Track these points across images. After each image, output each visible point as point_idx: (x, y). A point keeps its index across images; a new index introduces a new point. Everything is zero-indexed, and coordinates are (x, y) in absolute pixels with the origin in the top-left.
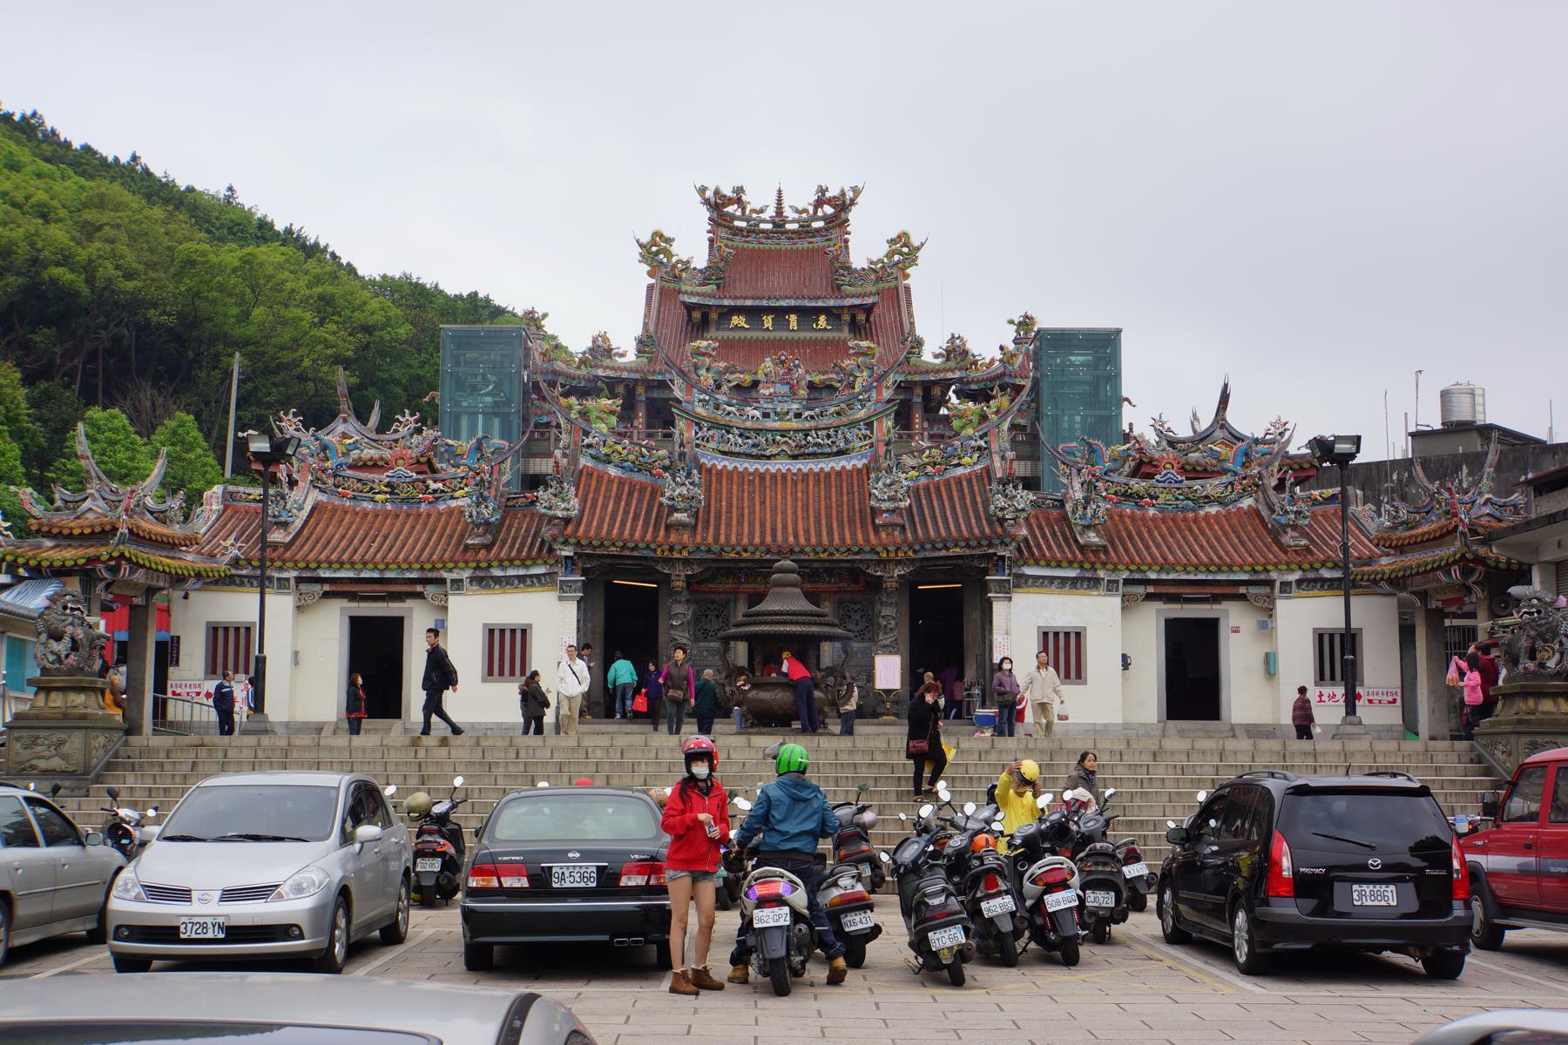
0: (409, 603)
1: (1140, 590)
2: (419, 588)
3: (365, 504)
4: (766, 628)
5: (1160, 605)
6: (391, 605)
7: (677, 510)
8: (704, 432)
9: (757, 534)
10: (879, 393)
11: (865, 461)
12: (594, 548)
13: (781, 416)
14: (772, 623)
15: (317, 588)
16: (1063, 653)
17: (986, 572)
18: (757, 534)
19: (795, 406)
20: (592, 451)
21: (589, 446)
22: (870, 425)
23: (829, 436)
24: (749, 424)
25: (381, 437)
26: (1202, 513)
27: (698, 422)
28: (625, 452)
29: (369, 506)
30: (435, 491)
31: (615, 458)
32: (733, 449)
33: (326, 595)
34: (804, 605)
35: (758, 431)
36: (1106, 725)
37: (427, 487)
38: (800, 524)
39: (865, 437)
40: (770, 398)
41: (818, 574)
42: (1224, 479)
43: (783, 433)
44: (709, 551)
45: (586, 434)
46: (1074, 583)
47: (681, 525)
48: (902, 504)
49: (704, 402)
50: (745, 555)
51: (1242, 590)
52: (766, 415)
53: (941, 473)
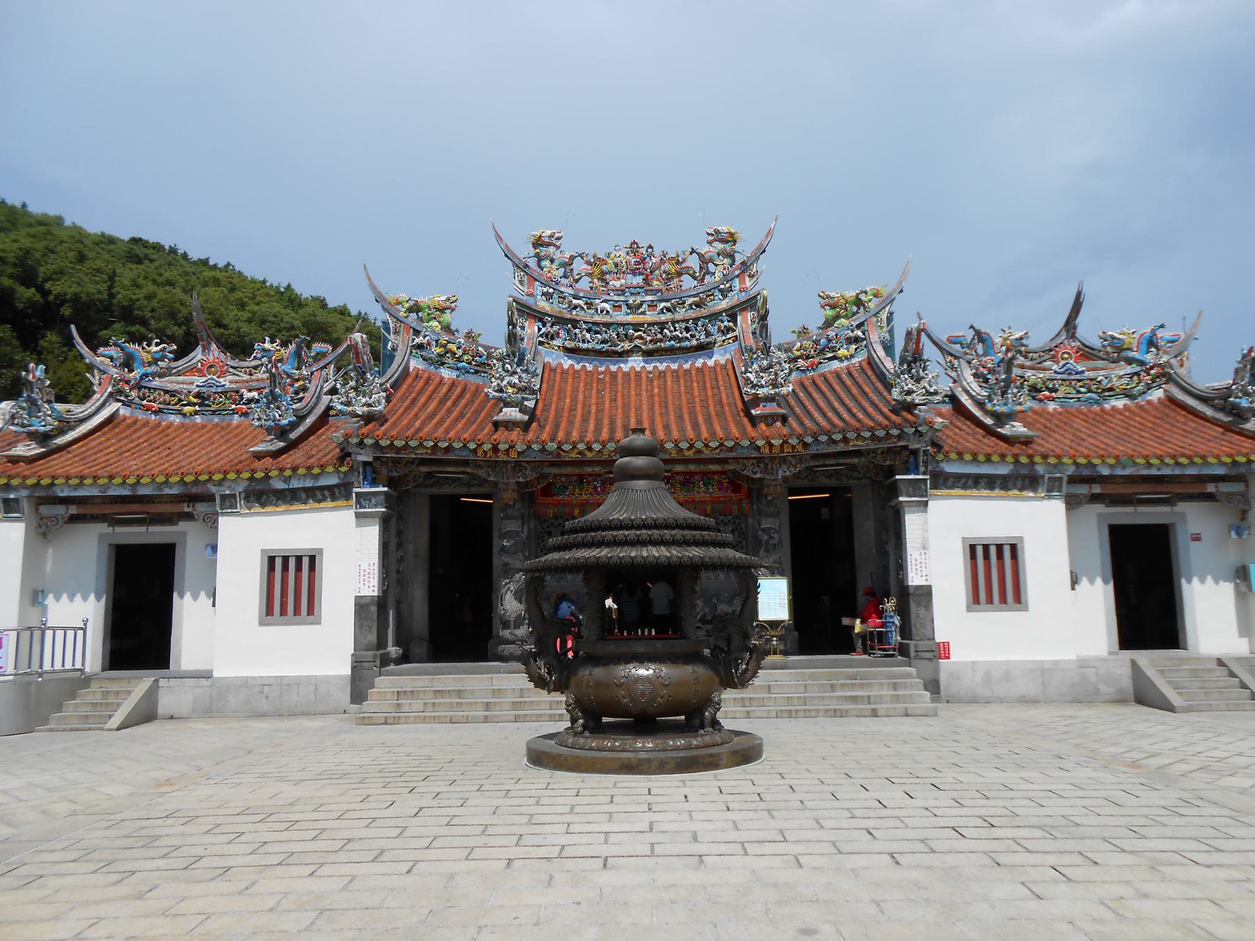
0: (183, 526)
1: (1083, 490)
3: (172, 417)
4: (604, 552)
5: (1100, 508)
6: (152, 529)
7: (507, 405)
9: (605, 430)
11: (728, 356)
14: (615, 543)
15: (60, 510)
16: (996, 573)
17: (891, 472)
18: (605, 430)
19: (649, 298)
21: (420, 347)
22: (733, 318)
24: (597, 318)
26: (1107, 406)
27: (539, 316)
28: (460, 352)
29: (177, 419)
30: (250, 401)
33: (74, 519)
35: (608, 325)
36: (1056, 663)
37: (241, 396)
38: (658, 419)
39: (728, 330)
40: (621, 291)
41: (680, 471)
43: (637, 327)
44: (543, 450)
45: (417, 333)
47: (509, 425)
48: (784, 390)
49: (548, 296)
50: (589, 455)
51: (1211, 488)
52: (617, 307)
53: (813, 367)
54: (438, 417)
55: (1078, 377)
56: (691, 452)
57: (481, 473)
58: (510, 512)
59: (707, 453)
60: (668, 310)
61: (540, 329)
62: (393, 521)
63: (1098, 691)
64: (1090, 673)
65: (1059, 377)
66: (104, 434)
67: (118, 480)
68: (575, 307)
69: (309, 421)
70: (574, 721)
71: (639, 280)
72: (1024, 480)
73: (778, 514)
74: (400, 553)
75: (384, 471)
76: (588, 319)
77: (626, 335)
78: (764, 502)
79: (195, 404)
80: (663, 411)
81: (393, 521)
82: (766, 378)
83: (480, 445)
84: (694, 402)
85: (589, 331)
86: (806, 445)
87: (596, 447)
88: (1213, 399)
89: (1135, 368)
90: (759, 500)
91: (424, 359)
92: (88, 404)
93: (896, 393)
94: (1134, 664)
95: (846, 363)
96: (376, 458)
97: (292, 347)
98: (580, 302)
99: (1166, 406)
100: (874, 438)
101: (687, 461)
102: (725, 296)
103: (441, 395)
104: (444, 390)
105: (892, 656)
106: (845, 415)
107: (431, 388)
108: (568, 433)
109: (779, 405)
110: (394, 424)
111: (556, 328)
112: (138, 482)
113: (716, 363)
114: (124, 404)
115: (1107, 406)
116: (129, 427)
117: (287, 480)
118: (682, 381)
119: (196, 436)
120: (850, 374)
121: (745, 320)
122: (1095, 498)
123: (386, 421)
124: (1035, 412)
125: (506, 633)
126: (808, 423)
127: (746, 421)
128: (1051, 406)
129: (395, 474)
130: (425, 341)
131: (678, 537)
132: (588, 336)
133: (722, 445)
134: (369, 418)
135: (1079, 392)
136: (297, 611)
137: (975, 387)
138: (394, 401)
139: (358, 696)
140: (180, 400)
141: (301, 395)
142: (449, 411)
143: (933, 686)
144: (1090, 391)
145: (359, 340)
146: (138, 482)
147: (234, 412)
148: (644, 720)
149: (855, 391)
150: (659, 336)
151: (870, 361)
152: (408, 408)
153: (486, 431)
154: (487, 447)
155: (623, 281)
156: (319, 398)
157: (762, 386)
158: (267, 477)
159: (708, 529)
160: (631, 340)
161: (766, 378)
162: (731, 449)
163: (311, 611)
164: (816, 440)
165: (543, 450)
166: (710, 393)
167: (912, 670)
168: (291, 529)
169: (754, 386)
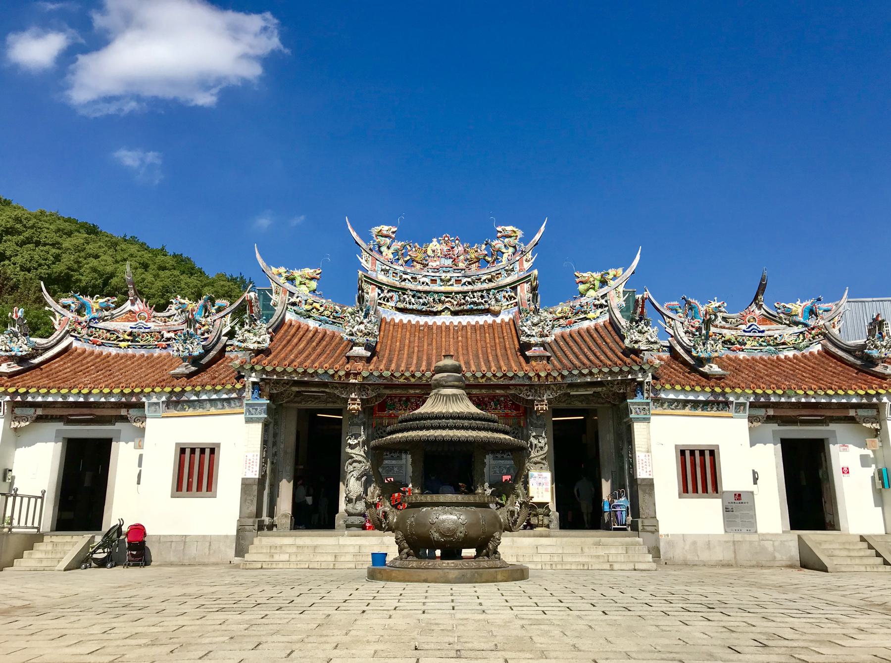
0: (119, 426)
1: (761, 412)
2: (123, 412)
4: (400, 435)
5: (774, 427)
8: (385, 294)
10: (521, 264)
12: (278, 374)
13: (445, 282)
15: (30, 411)
17: (624, 397)
20: (295, 308)
21: (294, 304)
22: (514, 289)
23: (482, 297)
24: (420, 288)
25: (159, 314)
27: (380, 286)
28: (322, 309)
30: (168, 339)
31: (314, 314)
32: (408, 306)
33: (40, 419)
34: (471, 408)
40: (436, 270)
41: (481, 392)
42: (796, 329)
43: (447, 294)
44: (381, 376)
46: (705, 405)
48: (548, 339)
49: (386, 272)
50: (413, 380)
51: (852, 413)
52: (434, 281)
54: (307, 352)
55: (760, 334)
56: (484, 380)
58: (356, 420)
59: (495, 381)
60: (469, 283)
61: (379, 295)
62: (271, 426)
63: (774, 559)
64: (768, 545)
65: (747, 334)
66: (62, 359)
67: (75, 391)
68: (405, 280)
69: (213, 353)
71: (449, 262)
72: (718, 404)
73: (545, 425)
74: (275, 450)
75: (267, 390)
77: (439, 300)
78: (534, 416)
79: (128, 340)
80: (465, 352)
81: (271, 426)
83: (336, 372)
84: (486, 347)
85: (413, 296)
86: (563, 377)
87: (418, 374)
88: (855, 351)
89: (801, 328)
90: (531, 416)
91: (296, 313)
92: (51, 338)
93: (627, 341)
94: (799, 537)
97: (201, 302)
98: (409, 277)
99: (823, 356)
100: (611, 373)
102: (509, 275)
103: (308, 338)
104: (310, 335)
105: (625, 529)
106: (592, 357)
107: (301, 333)
108: (398, 366)
109: (545, 349)
110: (275, 356)
111: (390, 294)
112: (90, 392)
113: (502, 320)
115: (782, 356)
116: (80, 355)
117: (197, 394)
118: (478, 332)
119: (129, 362)
120: (596, 329)
121: (522, 290)
122: (769, 419)
123: (270, 353)
124: (730, 359)
126: (565, 361)
127: (522, 359)
129: (275, 392)
130: (298, 300)
131: (474, 425)
132: (413, 300)
134: (258, 352)
135: (761, 345)
136: (199, 489)
137: (686, 339)
138: (275, 340)
139: (240, 551)
140: (118, 337)
141: (206, 335)
142: (314, 349)
143: (655, 552)
144: (770, 345)
145: (253, 297)
146: (90, 392)
147: (156, 347)
149: (599, 341)
150: (463, 301)
151: (612, 323)
152: (285, 346)
153: (341, 362)
154: (342, 373)
155: (438, 263)
156: (219, 338)
157: (533, 336)
158: (183, 391)
159: (494, 421)
160: (443, 302)
161: (537, 330)
162: (511, 378)
163: (209, 488)
164: (570, 373)
165: (381, 376)
166: (497, 341)
167: (640, 540)
168: (196, 429)
169: (528, 336)
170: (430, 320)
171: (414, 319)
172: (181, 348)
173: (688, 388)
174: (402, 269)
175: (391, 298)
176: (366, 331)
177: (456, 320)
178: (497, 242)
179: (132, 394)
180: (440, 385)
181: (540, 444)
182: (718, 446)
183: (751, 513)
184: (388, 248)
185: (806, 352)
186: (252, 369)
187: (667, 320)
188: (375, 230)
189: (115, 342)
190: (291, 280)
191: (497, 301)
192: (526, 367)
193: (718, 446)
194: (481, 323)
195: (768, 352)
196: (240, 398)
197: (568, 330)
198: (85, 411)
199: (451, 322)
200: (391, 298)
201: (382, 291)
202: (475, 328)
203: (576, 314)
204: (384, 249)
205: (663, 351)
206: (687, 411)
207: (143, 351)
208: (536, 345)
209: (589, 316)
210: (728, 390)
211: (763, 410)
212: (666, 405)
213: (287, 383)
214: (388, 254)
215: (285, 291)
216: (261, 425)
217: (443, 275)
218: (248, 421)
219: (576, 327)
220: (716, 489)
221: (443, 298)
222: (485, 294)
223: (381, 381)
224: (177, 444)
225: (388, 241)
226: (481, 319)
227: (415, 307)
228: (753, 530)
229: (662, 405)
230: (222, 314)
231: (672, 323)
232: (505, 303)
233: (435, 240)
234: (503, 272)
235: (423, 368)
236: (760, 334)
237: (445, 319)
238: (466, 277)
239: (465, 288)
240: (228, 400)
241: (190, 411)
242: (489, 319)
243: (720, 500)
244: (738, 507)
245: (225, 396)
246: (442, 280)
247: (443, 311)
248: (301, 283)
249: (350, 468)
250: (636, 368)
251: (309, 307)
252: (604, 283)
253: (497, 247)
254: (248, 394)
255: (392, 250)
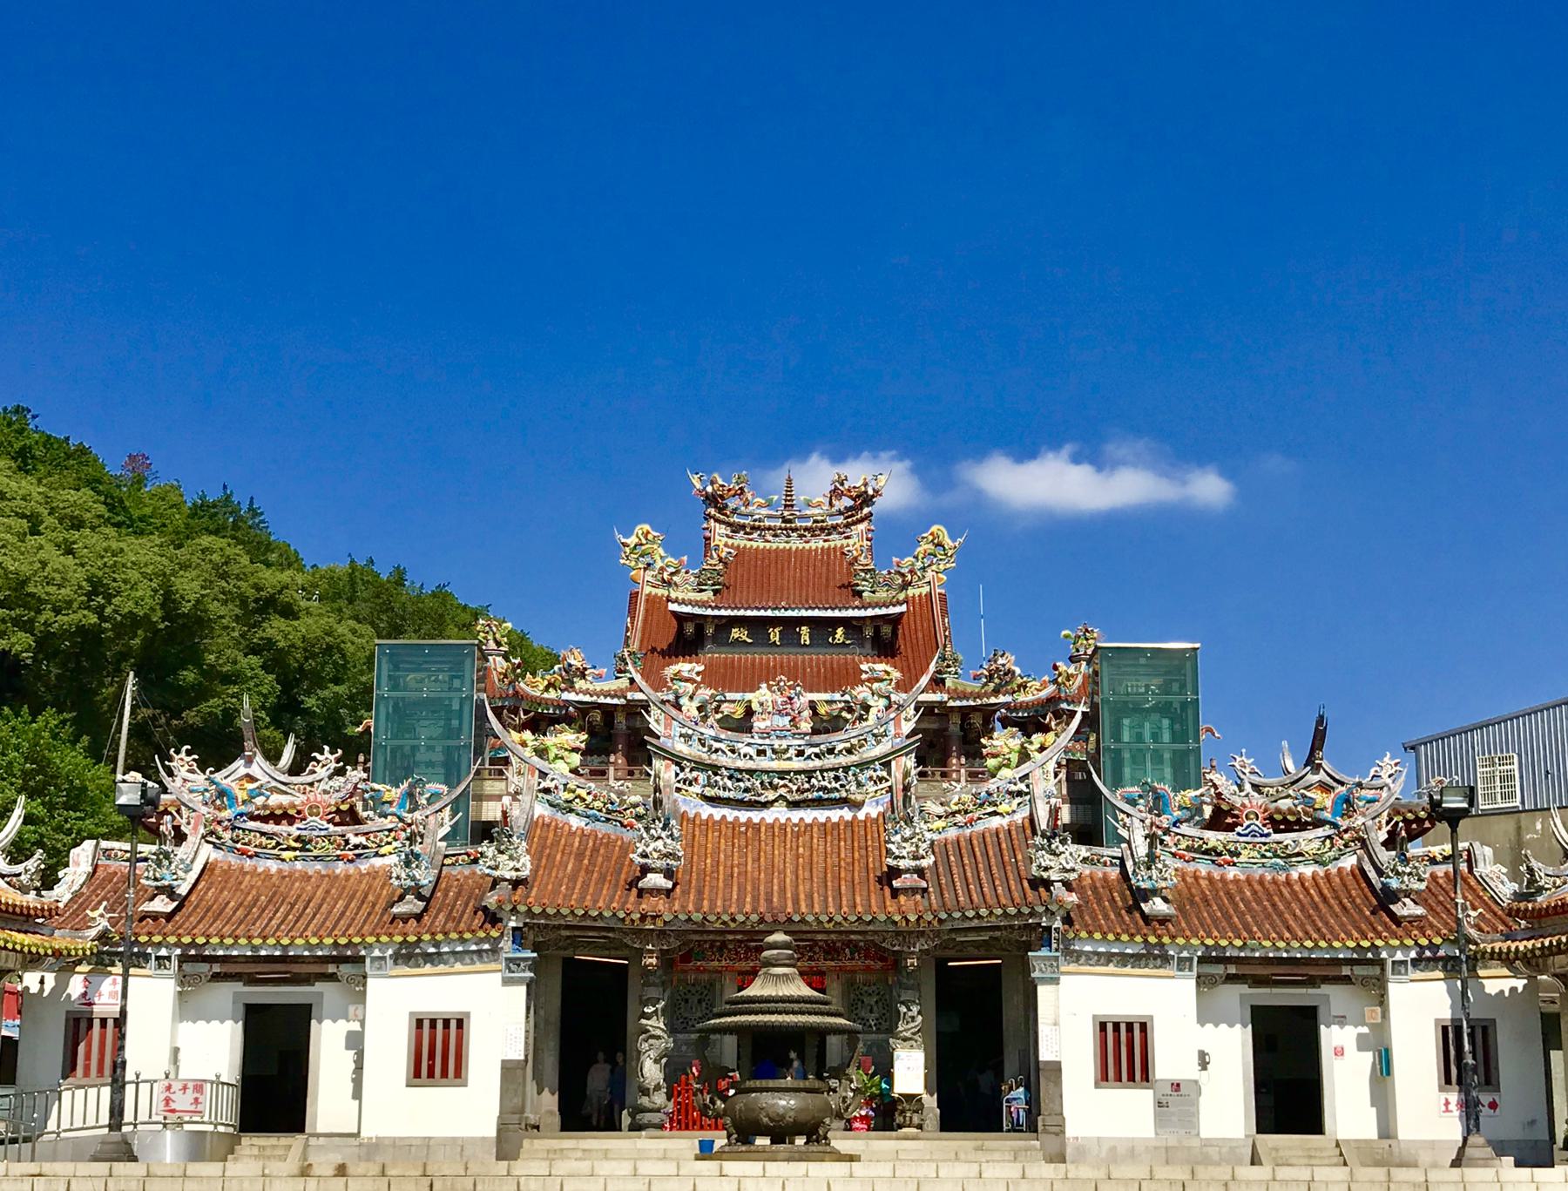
0: (319, 987)
1: (1219, 970)
3: (270, 863)
4: (729, 1019)
5: (1244, 989)
8: (687, 774)
10: (898, 725)
11: (881, 809)
15: (204, 968)
20: (547, 797)
21: (547, 791)
22: (887, 765)
24: (741, 764)
27: (678, 760)
28: (589, 799)
33: (216, 977)
34: (807, 991)
35: (751, 772)
37: (347, 842)
39: (881, 779)
40: (766, 734)
41: (819, 950)
42: (1320, 832)
43: (782, 774)
46: (1136, 960)
49: (687, 738)
50: (733, 925)
51: (1346, 971)
52: (761, 753)
57: (627, 940)
60: (817, 755)
67: (271, 941)
68: (717, 751)
70: (729, 1137)
72: (1153, 957)
75: (531, 937)
76: (730, 764)
79: (295, 849)
82: (909, 848)
85: (730, 778)
87: (740, 918)
95: (1007, 819)
96: (526, 924)
101: (828, 932)
102: (879, 742)
111: (695, 774)
114: (215, 846)
117: (437, 945)
122: (1231, 979)
125: (644, 1101)
128: (1231, 873)
132: (729, 783)
133: (860, 918)
134: (516, 883)
135: (1264, 856)
140: (278, 844)
147: (339, 858)
148: (781, 1132)
154: (636, 916)
155: (768, 723)
160: (775, 788)
163: (458, 1074)
166: (856, 855)
170: (756, 816)
171: (730, 814)
172: (403, 875)
173: (1111, 937)
174: (712, 733)
175: (696, 779)
176: (664, 851)
177: (796, 815)
178: (860, 688)
179: (350, 944)
180: (770, 963)
181: (914, 1017)
182: (1151, 1017)
183: (1193, 1109)
184: (691, 698)
185: (1332, 869)
186: (514, 910)
187: (1121, 816)
188: (670, 671)
189: (276, 851)
190: (541, 752)
191: (859, 785)
192: (891, 906)
193: (1151, 1017)
194: (835, 819)
195: (1273, 866)
196: (495, 951)
197: (968, 832)
198: (279, 967)
199: (789, 819)
200: (696, 779)
201: (682, 769)
202: (826, 828)
203: (981, 805)
204: (684, 701)
205: (1112, 864)
206: (1111, 968)
207: (318, 866)
208: (907, 871)
209: (1001, 809)
210: (1166, 940)
211: (1222, 967)
212: (1083, 959)
213: (559, 927)
214: (690, 707)
215: (533, 768)
216: (523, 989)
217: (777, 744)
218: (507, 982)
219: (980, 827)
220: (1146, 1077)
221: (776, 781)
222: (841, 774)
223: (689, 927)
224: (411, 1014)
225: (690, 687)
226: (835, 815)
227: (731, 795)
228: (1194, 1132)
229: (1077, 961)
230: (437, 806)
231: (1127, 821)
232: (871, 787)
233: (764, 685)
234: (870, 738)
235: (748, 908)
236: (1263, 840)
237: (779, 813)
238: (812, 746)
239: (811, 764)
240: (479, 952)
241: (428, 968)
242: (847, 814)
243: (1150, 1092)
244: (1177, 1101)
245: (474, 948)
246: (774, 751)
247: (776, 800)
248: (557, 757)
249: (645, 1046)
250: (1041, 909)
251: (570, 796)
252: (1024, 756)
253: (860, 697)
254: (507, 944)
255: (696, 704)
